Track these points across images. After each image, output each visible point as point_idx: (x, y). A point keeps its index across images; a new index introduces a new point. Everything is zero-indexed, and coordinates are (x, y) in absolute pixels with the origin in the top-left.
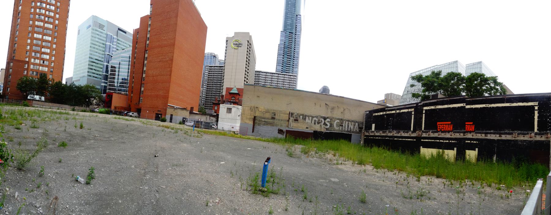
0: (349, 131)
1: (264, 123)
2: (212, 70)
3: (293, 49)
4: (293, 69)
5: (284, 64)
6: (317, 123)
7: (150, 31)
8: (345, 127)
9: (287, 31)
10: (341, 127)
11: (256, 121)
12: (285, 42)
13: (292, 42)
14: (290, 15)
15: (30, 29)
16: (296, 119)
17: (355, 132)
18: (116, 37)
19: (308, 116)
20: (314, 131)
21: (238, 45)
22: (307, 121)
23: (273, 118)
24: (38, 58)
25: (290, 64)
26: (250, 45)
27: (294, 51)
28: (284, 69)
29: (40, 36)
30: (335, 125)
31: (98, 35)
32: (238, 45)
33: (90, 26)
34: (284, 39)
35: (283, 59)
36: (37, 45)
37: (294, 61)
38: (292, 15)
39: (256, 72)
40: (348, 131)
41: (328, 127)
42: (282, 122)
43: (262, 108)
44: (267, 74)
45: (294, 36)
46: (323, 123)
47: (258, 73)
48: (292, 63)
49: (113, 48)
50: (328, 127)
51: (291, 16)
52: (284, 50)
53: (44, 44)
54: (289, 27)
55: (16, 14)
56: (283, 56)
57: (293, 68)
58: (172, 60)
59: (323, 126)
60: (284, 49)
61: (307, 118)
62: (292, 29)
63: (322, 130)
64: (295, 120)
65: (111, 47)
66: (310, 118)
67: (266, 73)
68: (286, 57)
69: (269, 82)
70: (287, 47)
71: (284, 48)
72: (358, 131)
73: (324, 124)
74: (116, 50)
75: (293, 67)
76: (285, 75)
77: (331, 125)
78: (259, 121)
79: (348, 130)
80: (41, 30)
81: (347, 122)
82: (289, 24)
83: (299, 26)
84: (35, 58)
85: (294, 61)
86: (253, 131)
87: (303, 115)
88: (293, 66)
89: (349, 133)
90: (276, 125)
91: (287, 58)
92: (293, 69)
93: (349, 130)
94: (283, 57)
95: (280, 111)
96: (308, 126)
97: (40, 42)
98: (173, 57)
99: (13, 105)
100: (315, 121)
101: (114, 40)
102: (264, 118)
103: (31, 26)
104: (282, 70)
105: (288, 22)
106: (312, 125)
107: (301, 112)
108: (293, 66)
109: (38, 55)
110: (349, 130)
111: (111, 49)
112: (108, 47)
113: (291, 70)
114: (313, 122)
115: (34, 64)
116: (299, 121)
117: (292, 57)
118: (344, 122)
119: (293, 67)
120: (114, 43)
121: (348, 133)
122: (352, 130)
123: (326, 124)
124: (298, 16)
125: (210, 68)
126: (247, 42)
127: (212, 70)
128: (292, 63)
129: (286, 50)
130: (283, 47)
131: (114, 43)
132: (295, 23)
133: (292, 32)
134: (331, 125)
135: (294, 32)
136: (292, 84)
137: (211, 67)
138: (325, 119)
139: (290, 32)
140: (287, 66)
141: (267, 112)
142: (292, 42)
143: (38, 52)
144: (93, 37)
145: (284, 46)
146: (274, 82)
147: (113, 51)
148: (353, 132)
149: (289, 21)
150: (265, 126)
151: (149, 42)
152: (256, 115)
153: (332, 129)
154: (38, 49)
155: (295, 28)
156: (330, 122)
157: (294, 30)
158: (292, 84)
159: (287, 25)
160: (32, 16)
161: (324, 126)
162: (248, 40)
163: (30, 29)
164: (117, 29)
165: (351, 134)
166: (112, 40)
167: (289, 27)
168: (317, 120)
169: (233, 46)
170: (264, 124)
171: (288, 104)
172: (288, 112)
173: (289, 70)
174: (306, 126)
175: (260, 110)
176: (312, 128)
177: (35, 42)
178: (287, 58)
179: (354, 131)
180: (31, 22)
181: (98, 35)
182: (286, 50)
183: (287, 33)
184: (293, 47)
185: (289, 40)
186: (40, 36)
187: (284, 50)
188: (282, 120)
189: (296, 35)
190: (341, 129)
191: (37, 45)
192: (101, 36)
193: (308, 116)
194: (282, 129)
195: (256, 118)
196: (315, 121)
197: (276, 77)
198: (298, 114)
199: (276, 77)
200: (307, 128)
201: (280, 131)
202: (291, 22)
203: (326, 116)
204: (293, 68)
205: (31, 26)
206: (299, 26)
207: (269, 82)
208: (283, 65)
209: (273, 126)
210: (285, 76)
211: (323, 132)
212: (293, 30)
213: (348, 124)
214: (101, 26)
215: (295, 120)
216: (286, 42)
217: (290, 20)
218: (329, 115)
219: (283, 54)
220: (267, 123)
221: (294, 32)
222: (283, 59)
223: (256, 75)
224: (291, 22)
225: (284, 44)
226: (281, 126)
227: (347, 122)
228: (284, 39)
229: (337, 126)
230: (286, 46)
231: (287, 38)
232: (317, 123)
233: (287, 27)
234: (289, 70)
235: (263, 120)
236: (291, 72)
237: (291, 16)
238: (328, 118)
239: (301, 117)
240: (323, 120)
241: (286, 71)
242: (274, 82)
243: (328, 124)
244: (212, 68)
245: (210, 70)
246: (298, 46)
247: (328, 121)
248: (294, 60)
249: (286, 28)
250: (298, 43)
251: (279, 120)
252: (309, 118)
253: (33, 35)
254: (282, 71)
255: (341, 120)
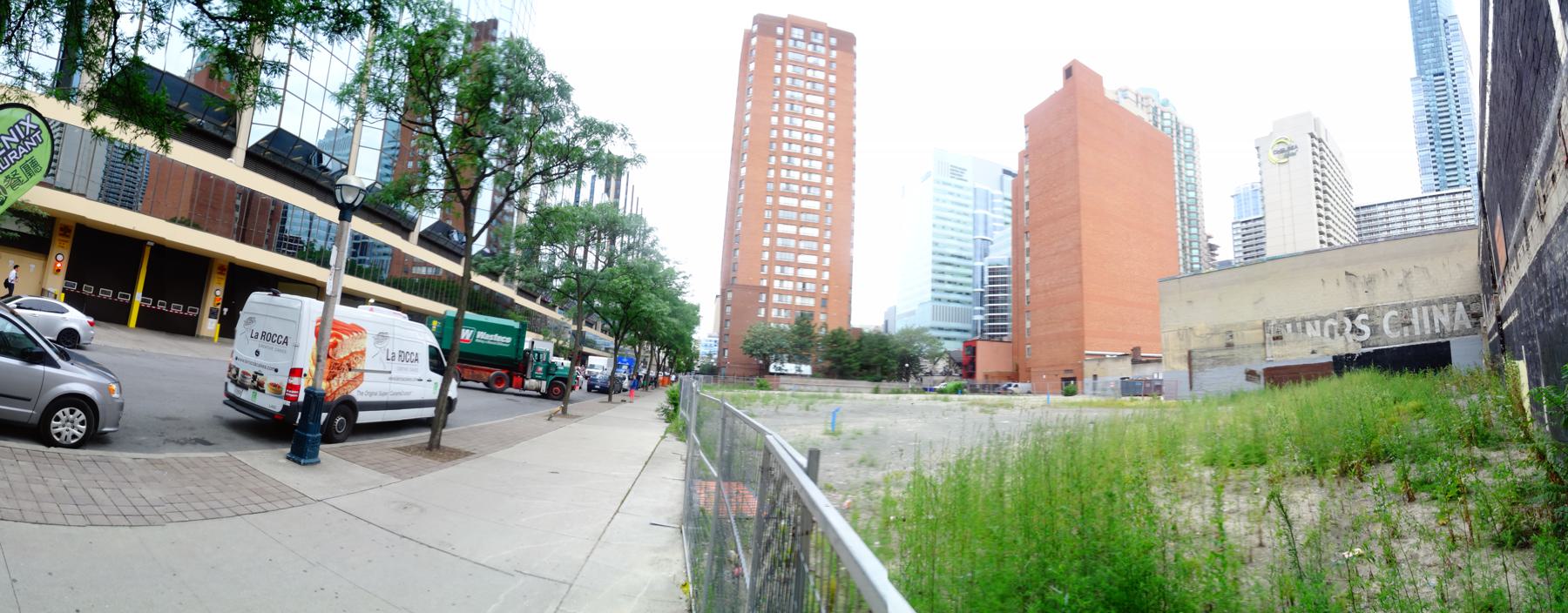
0: (1438, 335)
1: (1212, 361)
2: (1249, 231)
3: (1455, 118)
4: (1467, 172)
5: (1439, 167)
6: (1337, 335)
7: (1028, 187)
8: (1421, 325)
9: (1427, 72)
10: (1406, 329)
11: (1194, 362)
12: (1427, 106)
13: (1446, 98)
14: (1424, 26)
15: (768, 214)
16: (1276, 335)
17: (1459, 331)
18: (1000, 193)
19: (1310, 320)
20: (1334, 358)
21: (1287, 152)
22: (1309, 334)
23: (1230, 345)
24: (788, 278)
25: (1454, 163)
26: (1317, 141)
27: (1460, 120)
28: (1441, 178)
29: (792, 229)
30: (1386, 327)
31: (951, 194)
32: (1287, 152)
33: (928, 175)
34: (1422, 97)
35: (1433, 153)
36: (785, 249)
37: (1464, 149)
38: (1429, 25)
39: (1357, 209)
40: (1434, 335)
41: (1366, 336)
42: (1251, 350)
43: (1201, 327)
44: (1389, 207)
45: (1449, 80)
46: (1348, 329)
47: (1364, 214)
48: (1459, 158)
49: (994, 220)
50: (1366, 336)
51: (1428, 29)
52: (1429, 128)
53: (802, 245)
54: (1431, 60)
55: (736, 182)
56: (1432, 144)
57: (1467, 169)
58: (1079, 246)
59: (1351, 337)
60: (1430, 125)
61: (1308, 325)
62: (1439, 63)
63: (1351, 351)
64: (1275, 339)
65: (989, 220)
66: (1317, 323)
67: (1402, 201)
68: (1439, 146)
69: (1399, 225)
70: (1436, 116)
71: (1429, 122)
72: (1469, 326)
73: (1352, 332)
74: (1002, 225)
75: (1466, 166)
76: (1454, 194)
77: (1375, 330)
78: (1200, 360)
79: (1433, 331)
80: (793, 215)
81: (1425, 309)
82: (1429, 50)
83: (1458, 48)
84: (782, 279)
85: (1464, 149)
86: (1191, 387)
87: (1293, 321)
88: (1466, 163)
89: (1440, 340)
90: (1240, 362)
91: (1444, 146)
92: (1467, 172)
93: (1438, 331)
94: (1433, 147)
95: (1243, 325)
96: (1315, 348)
97: (792, 243)
98: (1080, 238)
99: (734, 388)
100: (1331, 327)
101: (995, 201)
102: (1211, 350)
103: (770, 208)
104: (1437, 182)
105: (1424, 46)
106: (1325, 340)
107: (1286, 314)
108: (1466, 163)
109: (790, 271)
110: (1438, 331)
111: (990, 225)
112: (981, 220)
113: (1462, 176)
114: (1327, 333)
115: (782, 292)
116: (1285, 339)
117: (1458, 140)
118: (1415, 311)
119: (1466, 166)
120: (995, 209)
121: (1435, 341)
122: (1448, 329)
123: (1360, 331)
124: (1450, 21)
125: (1244, 225)
126: (1309, 137)
127: (1249, 231)
128: (1459, 158)
129: (1434, 126)
130: (1426, 119)
131: (995, 209)
132: (1444, 44)
133: (1440, 70)
134: (1375, 330)
135: (1447, 69)
136: (1463, 216)
137: (1246, 222)
138: (1352, 316)
139: (1436, 71)
140: (1448, 170)
141: (1214, 333)
142: (1446, 98)
143: (788, 264)
144: (938, 200)
145: (1428, 116)
146: (1411, 223)
147: (995, 228)
148: (1452, 334)
149: (1426, 43)
150: (1215, 369)
151: (1031, 214)
152: (1192, 348)
153: (1380, 342)
154: (790, 257)
155: (1446, 54)
156: (1370, 320)
157: (1446, 63)
158: (1463, 216)
159: (1424, 57)
160: (770, 186)
161: (1354, 335)
162: (1313, 131)
163: (768, 214)
164: (1001, 173)
165: (1448, 343)
166: (990, 201)
167: (1431, 60)
168: (1335, 324)
169: (1275, 158)
170: (1213, 365)
171: (1256, 303)
172: (1261, 323)
173: (1456, 178)
174: (1310, 348)
175: (1198, 333)
176: (1327, 351)
177: (780, 242)
178: (1444, 146)
179: (1456, 329)
180: (769, 200)
181: (951, 194)
182: (1434, 126)
183: (1428, 78)
184: (1454, 112)
185: (1438, 97)
186: (792, 229)
187: (1429, 128)
188: (1249, 346)
189: (1454, 75)
190: (1406, 335)
191: (785, 249)
192: (959, 195)
193: (1310, 320)
194: (1253, 368)
195: (1193, 354)
196: (1331, 327)
197: (1414, 210)
198: (1279, 321)
199: (1414, 210)
200: (1313, 352)
201: (1251, 375)
202: (1433, 45)
203: (1353, 307)
204: (1467, 169)
205: (770, 208)
206: (1458, 48)
207: (1399, 225)
208: (1435, 170)
209: (1232, 364)
210: (1440, 198)
211: (1353, 355)
212: (1444, 64)
213: (1430, 312)
214: (957, 172)
215: (1275, 339)
216: (1431, 104)
217: (1428, 40)
218: (1362, 301)
219: (1431, 138)
220: (1217, 361)
221: (1447, 69)
222: (1433, 153)
223: (1362, 218)
224: (1433, 45)
225: (1427, 111)
226: (1251, 360)
227: (1425, 309)
228: (1422, 97)
229: (1393, 327)
230: (1432, 114)
231: (1430, 93)
232: (1337, 335)
233: (1426, 62)
234: (1456, 178)
235: (1209, 354)
236: (1463, 181)
237: (1428, 29)
238: (1360, 311)
239: (1289, 326)
240: (1347, 321)
241: (1449, 185)
242: (1411, 223)
243: (1366, 329)
244: (1250, 224)
245: (1245, 232)
246: (1466, 106)
247: (1363, 321)
248: (1464, 146)
249: (1422, 67)
250: (1465, 96)
251: (1243, 347)
252: (1313, 324)
253: (774, 228)
254: (1438, 188)
255: (1404, 307)
